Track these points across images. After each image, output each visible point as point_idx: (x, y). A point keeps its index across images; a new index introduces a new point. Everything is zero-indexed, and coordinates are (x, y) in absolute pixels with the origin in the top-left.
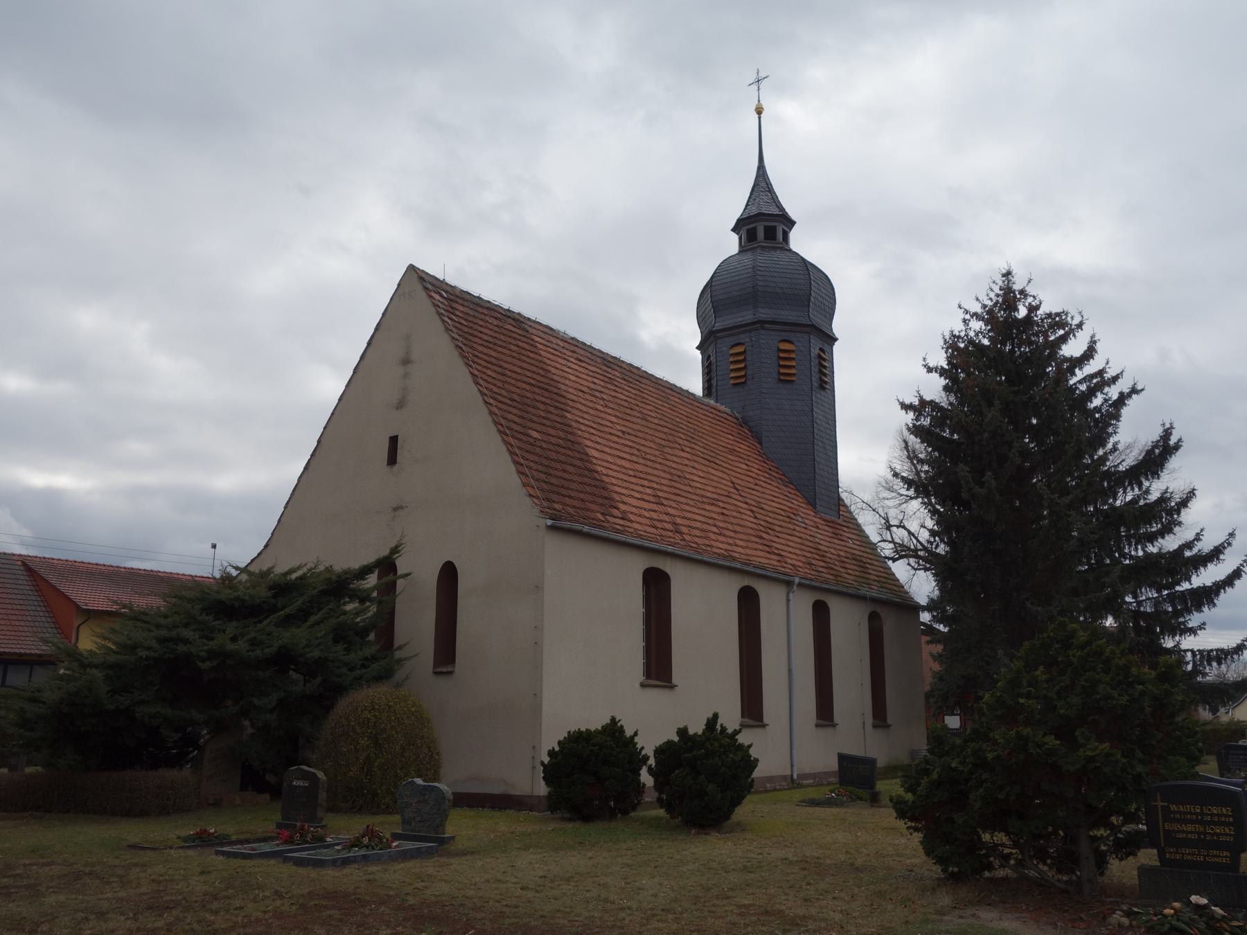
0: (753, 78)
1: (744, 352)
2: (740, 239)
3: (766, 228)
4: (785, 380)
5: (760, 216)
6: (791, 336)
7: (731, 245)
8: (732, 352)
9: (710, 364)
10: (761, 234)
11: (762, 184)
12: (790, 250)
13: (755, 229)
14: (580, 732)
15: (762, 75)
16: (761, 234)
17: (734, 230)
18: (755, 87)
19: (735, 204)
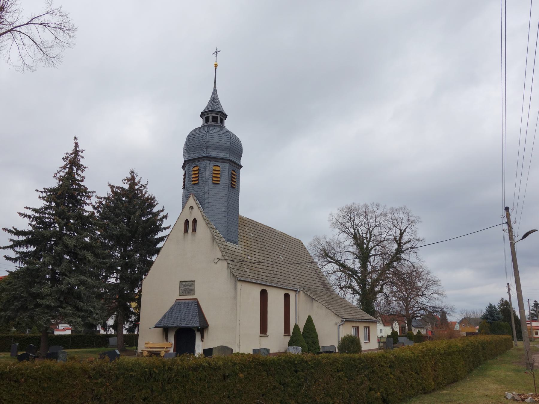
11: (214, 99)
15: (218, 50)
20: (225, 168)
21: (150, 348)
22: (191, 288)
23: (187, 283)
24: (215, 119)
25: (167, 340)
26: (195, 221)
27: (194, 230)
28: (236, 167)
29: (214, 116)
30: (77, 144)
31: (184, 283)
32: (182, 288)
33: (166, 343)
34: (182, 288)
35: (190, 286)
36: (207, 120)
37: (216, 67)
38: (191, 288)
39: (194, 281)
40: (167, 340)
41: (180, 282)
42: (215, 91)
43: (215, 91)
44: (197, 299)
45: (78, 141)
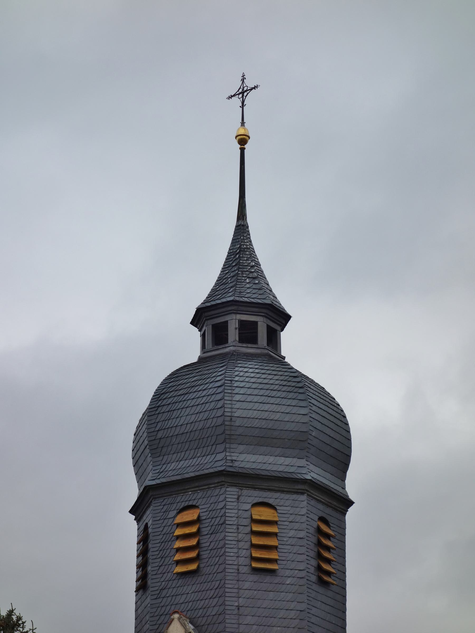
0: (235, 87)
1: (198, 520)
2: (203, 336)
3: (242, 323)
4: (264, 571)
5: (237, 306)
6: (271, 497)
7: (189, 346)
8: (180, 519)
9: (146, 527)
10: (233, 334)
11: (241, 255)
12: (281, 361)
13: (225, 325)
14: (248, 227)
15: (249, 83)
16: (233, 334)
17: (131, 512)
18: (237, 101)
19: (200, 285)
24: (248, 333)
42: (242, 229)
43: (242, 229)
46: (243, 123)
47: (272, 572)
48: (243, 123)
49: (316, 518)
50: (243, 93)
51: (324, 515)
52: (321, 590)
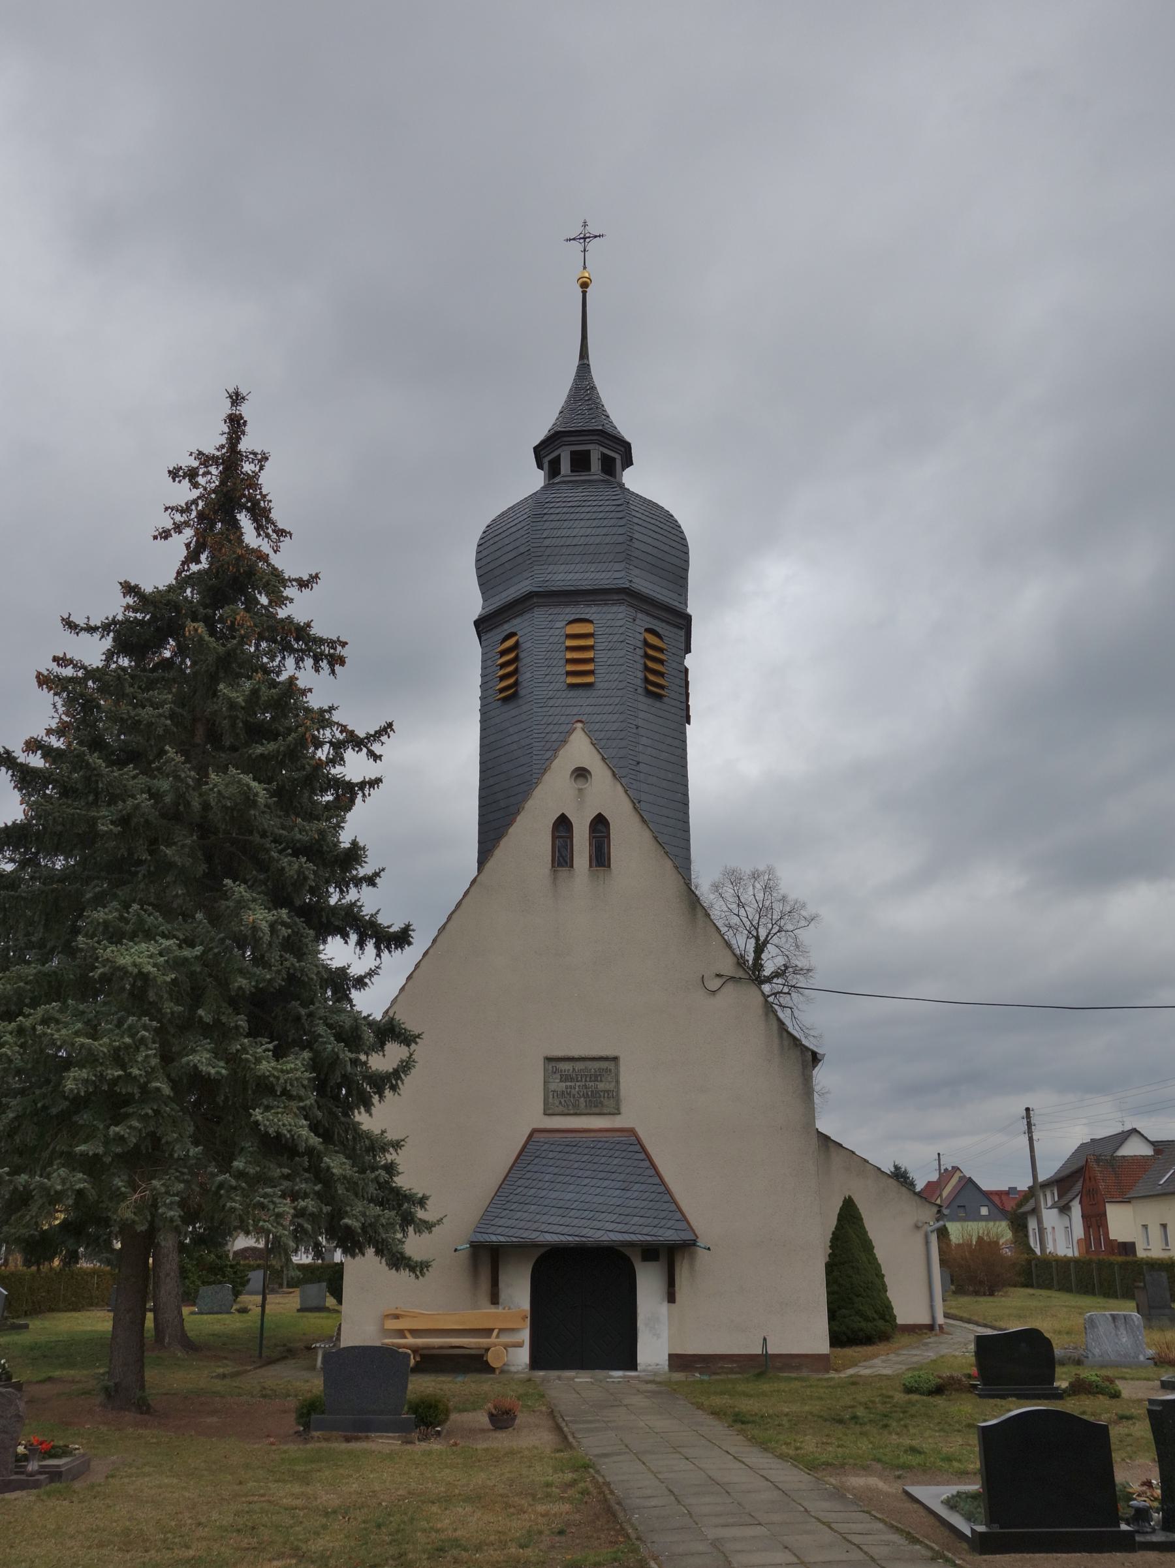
11: (583, 390)
15: (593, 230)
18: (577, 246)
20: (617, 631)
21: (415, 1332)
22: (601, 1086)
23: (579, 1066)
24: (580, 462)
25: (495, 1300)
26: (600, 824)
27: (601, 858)
28: (669, 623)
29: (584, 449)
30: (236, 424)
31: (566, 1067)
32: (558, 1085)
33: (493, 1310)
34: (558, 1085)
35: (597, 1077)
36: (553, 470)
37: (585, 285)
38: (601, 1086)
39: (615, 1059)
40: (495, 1300)
41: (549, 1059)
42: (584, 368)
43: (584, 368)
44: (632, 1132)
45: (245, 410)
46: (585, 268)
47: (589, 686)
48: (585, 268)
49: (642, 630)
50: (584, 238)
51: (650, 626)
52: (644, 702)
